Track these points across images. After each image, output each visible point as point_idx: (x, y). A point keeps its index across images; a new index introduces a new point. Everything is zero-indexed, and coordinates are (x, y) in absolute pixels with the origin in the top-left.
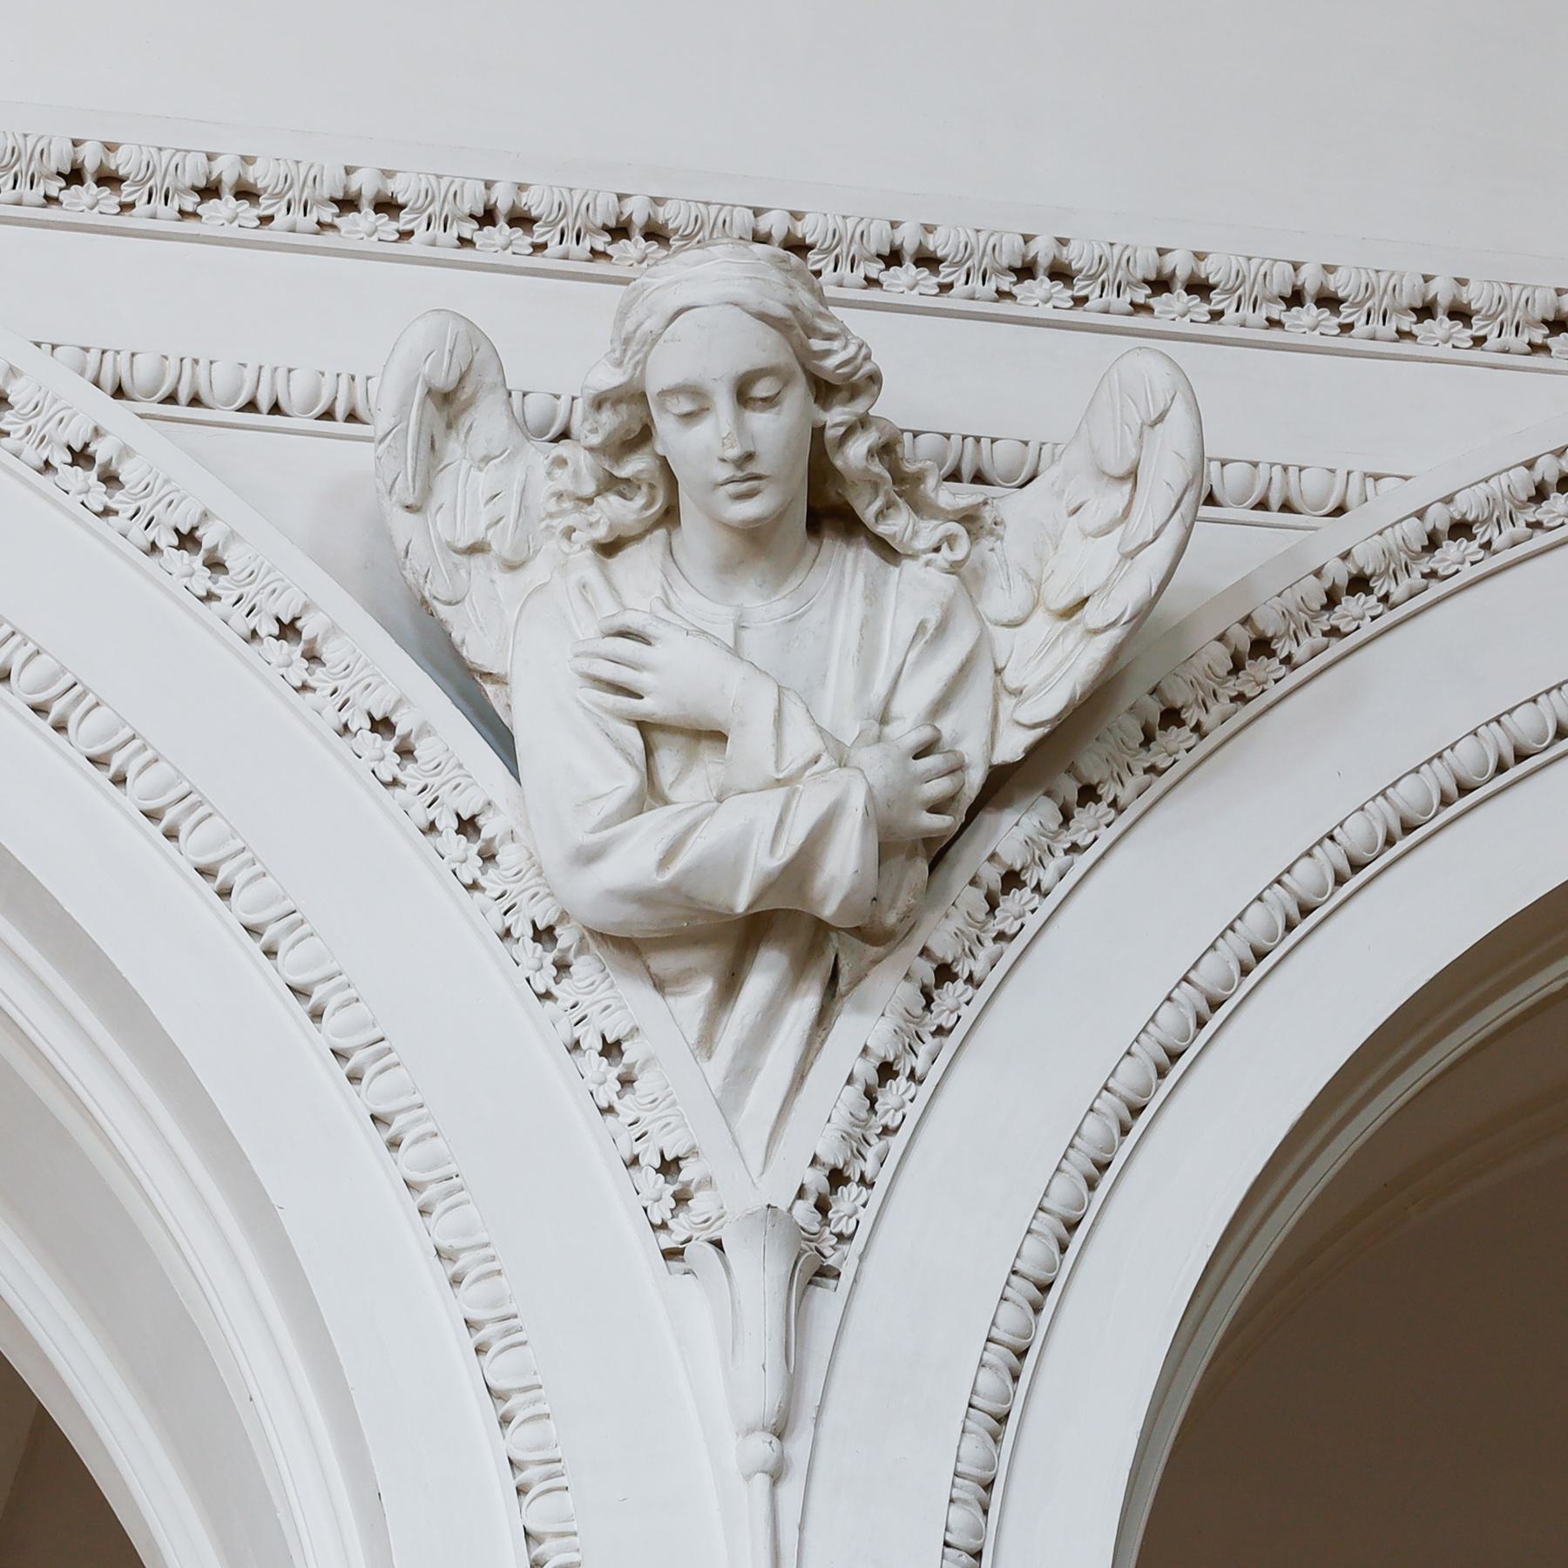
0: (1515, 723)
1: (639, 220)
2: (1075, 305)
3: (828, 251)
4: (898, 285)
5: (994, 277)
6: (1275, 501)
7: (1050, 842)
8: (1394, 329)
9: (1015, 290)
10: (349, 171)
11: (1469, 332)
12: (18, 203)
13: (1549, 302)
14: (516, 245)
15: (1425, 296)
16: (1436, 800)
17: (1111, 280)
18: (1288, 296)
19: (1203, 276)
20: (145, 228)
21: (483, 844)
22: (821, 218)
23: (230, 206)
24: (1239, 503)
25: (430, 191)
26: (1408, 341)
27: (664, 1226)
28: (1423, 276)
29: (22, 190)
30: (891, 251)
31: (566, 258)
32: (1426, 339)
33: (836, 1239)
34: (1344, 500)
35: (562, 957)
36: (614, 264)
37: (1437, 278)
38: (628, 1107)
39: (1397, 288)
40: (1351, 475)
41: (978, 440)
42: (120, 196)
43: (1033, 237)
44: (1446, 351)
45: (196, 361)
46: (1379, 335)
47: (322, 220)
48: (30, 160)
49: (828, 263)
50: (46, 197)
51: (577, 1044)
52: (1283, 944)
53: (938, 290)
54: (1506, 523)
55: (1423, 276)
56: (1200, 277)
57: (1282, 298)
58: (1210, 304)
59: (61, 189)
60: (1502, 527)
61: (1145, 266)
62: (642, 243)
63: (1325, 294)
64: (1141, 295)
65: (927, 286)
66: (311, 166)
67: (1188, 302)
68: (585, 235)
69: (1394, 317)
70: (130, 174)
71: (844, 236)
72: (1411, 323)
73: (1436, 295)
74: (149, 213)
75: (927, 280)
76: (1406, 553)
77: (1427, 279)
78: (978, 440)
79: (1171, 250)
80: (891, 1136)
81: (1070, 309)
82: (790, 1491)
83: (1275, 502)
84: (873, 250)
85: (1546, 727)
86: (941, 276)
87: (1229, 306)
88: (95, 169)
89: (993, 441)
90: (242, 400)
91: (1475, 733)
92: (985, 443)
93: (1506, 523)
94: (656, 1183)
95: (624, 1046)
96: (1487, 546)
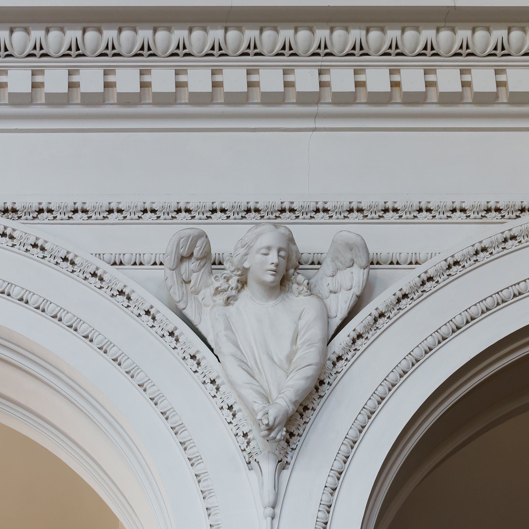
0: (471, 311)
1: (287, 208)
2: (330, 218)
3: (128, 211)
4: (146, 218)
5: (343, 213)
6: (414, 262)
7: (393, 307)
8: (171, 216)
9: (348, 216)
10: (109, 203)
11: (226, 215)
12: (235, 219)
13: (417, 205)
14: (497, 216)
15: (453, 207)
16: (451, 331)
17: (236, 211)
18: (315, 210)
19: (85, 208)
20: (315, 222)
21: (197, 361)
22: (159, 203)
23: (219, 214)
24: (148, 263)
25: (233, 206)
26: (175, 219)
27: (245, 450)
28: (487, 202)
29: (62, 216)
30: (316, 209)
31: (27, 220)
32: (351, 218)
33: (291, 450)
34: (392, 260)
35: (218, 387)
36: (453, 219)
37: (250, 202)
38: (234, 422)
39: (240, 206)
40: (216, 254)
41: (100, 254)
42: (191, 214)
43: (387, 202)
44: (46, 221)
45: (416, 254)
46: (306, 218)
47: (104, 216)
48: (202, 208)
49: (266, 213)
50: (447, 216)
51: (222, 407)
52: (412, 369)
53: (157, 218)
54: (468, 261)
55: (487, 202)
56: (498, 207)
57: (417, 210)
58: (191, 214)
59: (245, 214)
60: (467, 262)
61: (106, 207)
62: (289, 213)
63: (428, 209)
64: (278, 214)
65: (120, 217)
66: (272, 203)
67: (221, 215)
68: (274, 213)
69: (412, 213)
70: (365, 209)
71: (372, 206)
72: (175, 214)
73: (353, 207)
74: (336, 218)
75: (429, 215)
76: (442, 270)
77: (75, 203)
78: (416, 254)
79: (388, 202)
80: (306, 424)
81: (295, 219)
82: (276, 520)
83: (138, 263)
84: (312, 210)
85: (479, 312)
86: (54, 214)
87: (231, 214)
88: (322, 208)
89: (103, 254)
90: (152, 262)
91: (460, 314)
92: (142, 255)
93: (468, 261)
94: (242, 439)
95: (233, 406)
96: (464, 267)
